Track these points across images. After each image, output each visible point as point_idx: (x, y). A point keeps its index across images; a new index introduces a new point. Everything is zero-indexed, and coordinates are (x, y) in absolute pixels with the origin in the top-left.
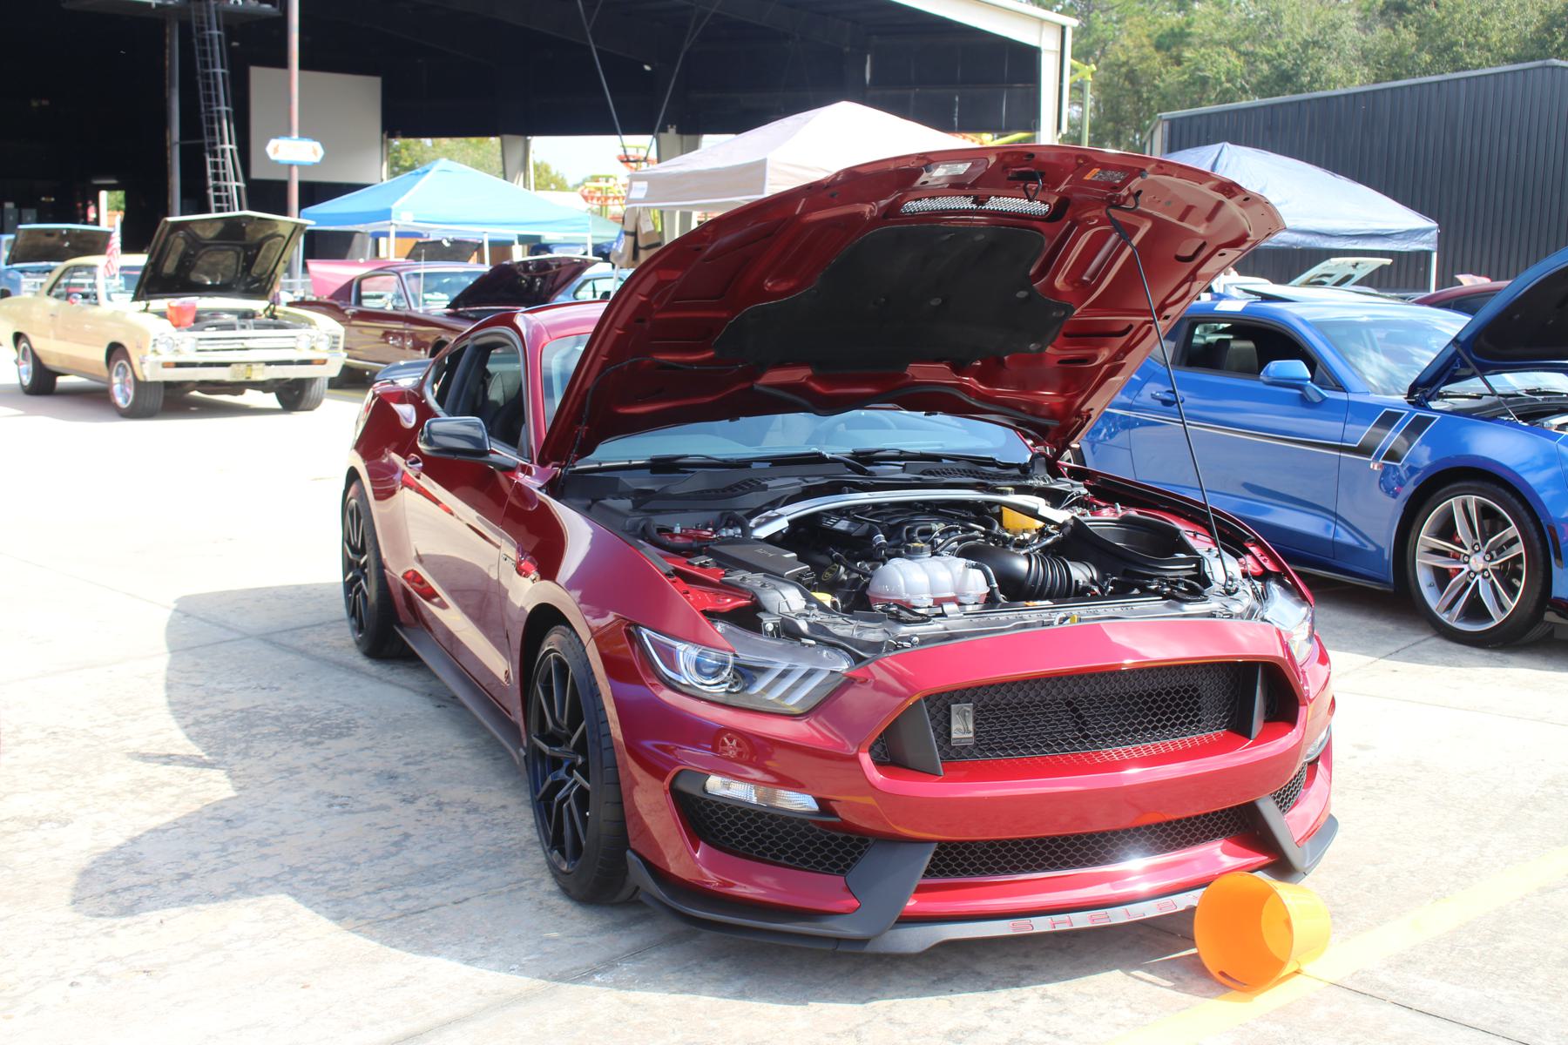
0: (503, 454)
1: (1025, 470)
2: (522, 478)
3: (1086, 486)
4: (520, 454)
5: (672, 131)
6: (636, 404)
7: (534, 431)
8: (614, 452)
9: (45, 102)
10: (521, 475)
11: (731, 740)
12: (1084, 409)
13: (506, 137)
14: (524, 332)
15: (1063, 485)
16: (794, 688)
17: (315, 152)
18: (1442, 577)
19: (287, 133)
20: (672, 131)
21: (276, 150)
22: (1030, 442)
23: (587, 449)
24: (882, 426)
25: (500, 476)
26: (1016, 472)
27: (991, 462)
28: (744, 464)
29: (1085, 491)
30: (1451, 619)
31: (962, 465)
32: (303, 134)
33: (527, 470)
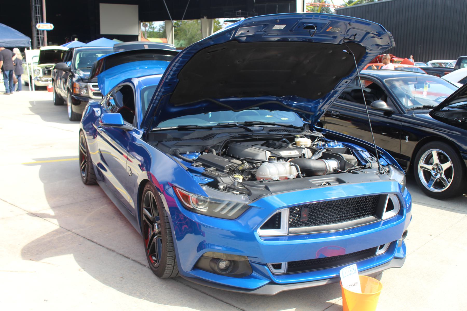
0: (128, 126)
1: (302, 129)
2: (135, 135)
3: (323, 134)
4: (134, 126)
5: (205, 18)
6: (241, 101)
7: (139, 117)
8: (165, 125)
9: (60, 15)
10: (134, 133)
11: (443, 160)
12: (322, 109)
13: (166, 21)
14: (136, 85)
15: (315, 134)
16: (223, 209)
17: (51, 27)
18: (427, 174)
19: (42, 22)
20: (205, 18)
21: (39, 27)
22: (303, 119)
23: (156, 125)
24: (255, 114)
25: (127, 132)
26: (299, 130)
27: (292, 126)
28: (210, 128)
29: (322, 136)
30: (432, 189)
31: (283, 128)
32: (48, 21)
33: (137, 132)
